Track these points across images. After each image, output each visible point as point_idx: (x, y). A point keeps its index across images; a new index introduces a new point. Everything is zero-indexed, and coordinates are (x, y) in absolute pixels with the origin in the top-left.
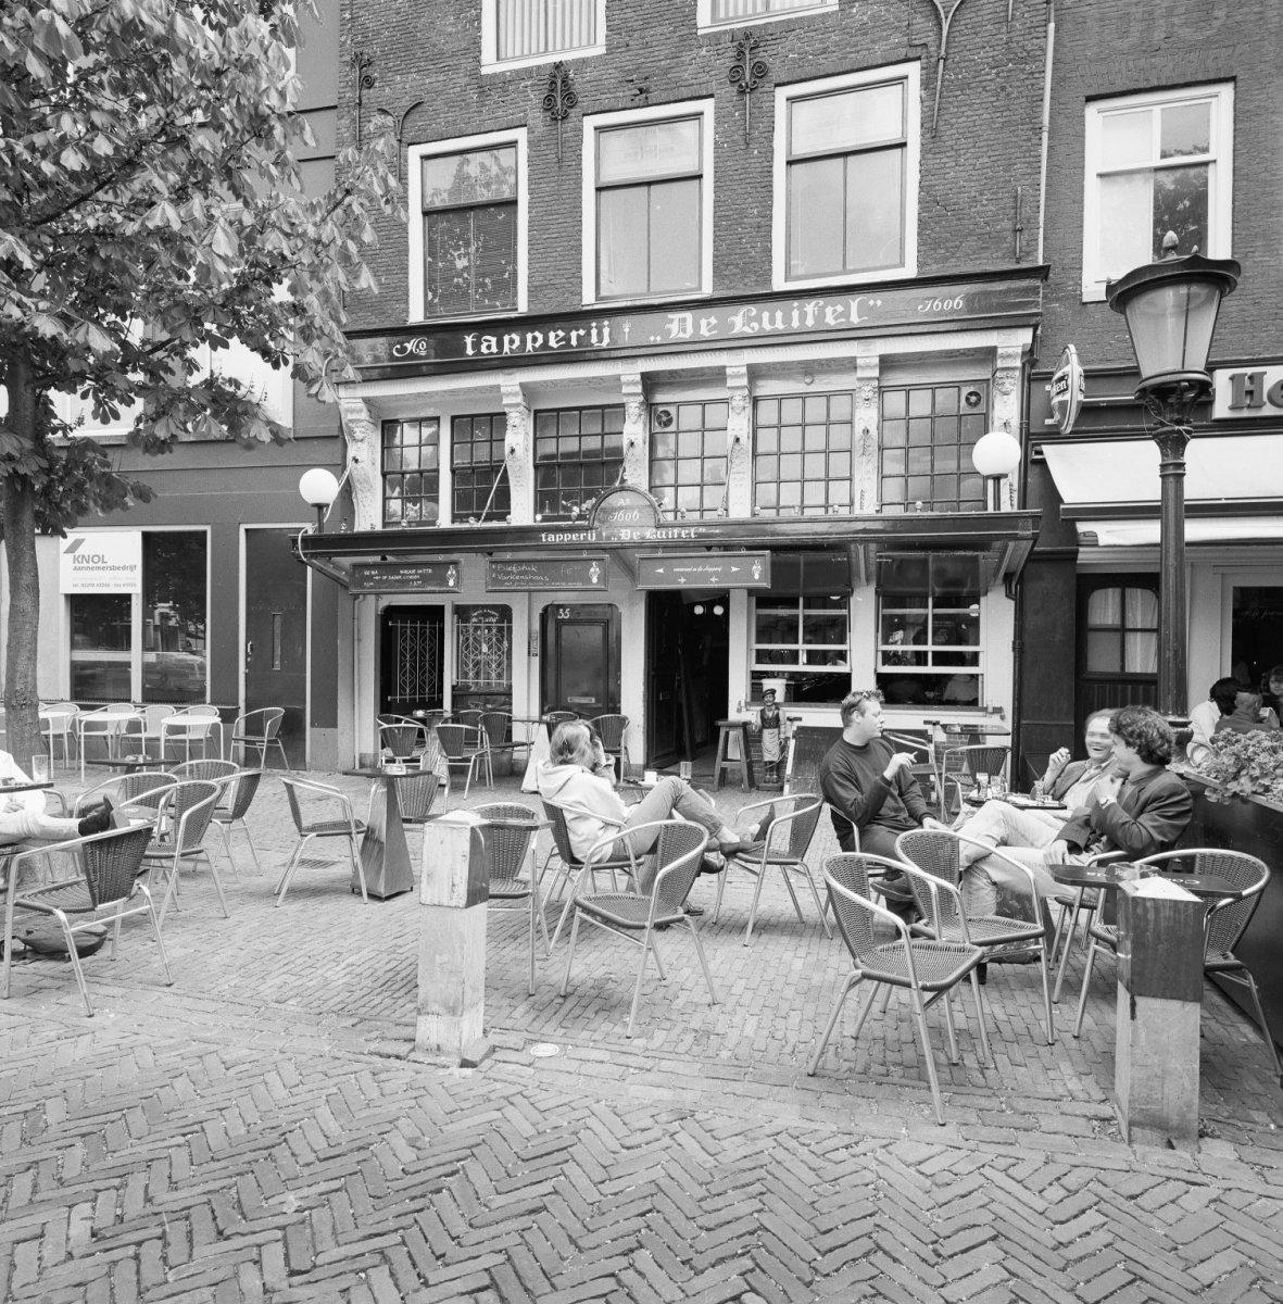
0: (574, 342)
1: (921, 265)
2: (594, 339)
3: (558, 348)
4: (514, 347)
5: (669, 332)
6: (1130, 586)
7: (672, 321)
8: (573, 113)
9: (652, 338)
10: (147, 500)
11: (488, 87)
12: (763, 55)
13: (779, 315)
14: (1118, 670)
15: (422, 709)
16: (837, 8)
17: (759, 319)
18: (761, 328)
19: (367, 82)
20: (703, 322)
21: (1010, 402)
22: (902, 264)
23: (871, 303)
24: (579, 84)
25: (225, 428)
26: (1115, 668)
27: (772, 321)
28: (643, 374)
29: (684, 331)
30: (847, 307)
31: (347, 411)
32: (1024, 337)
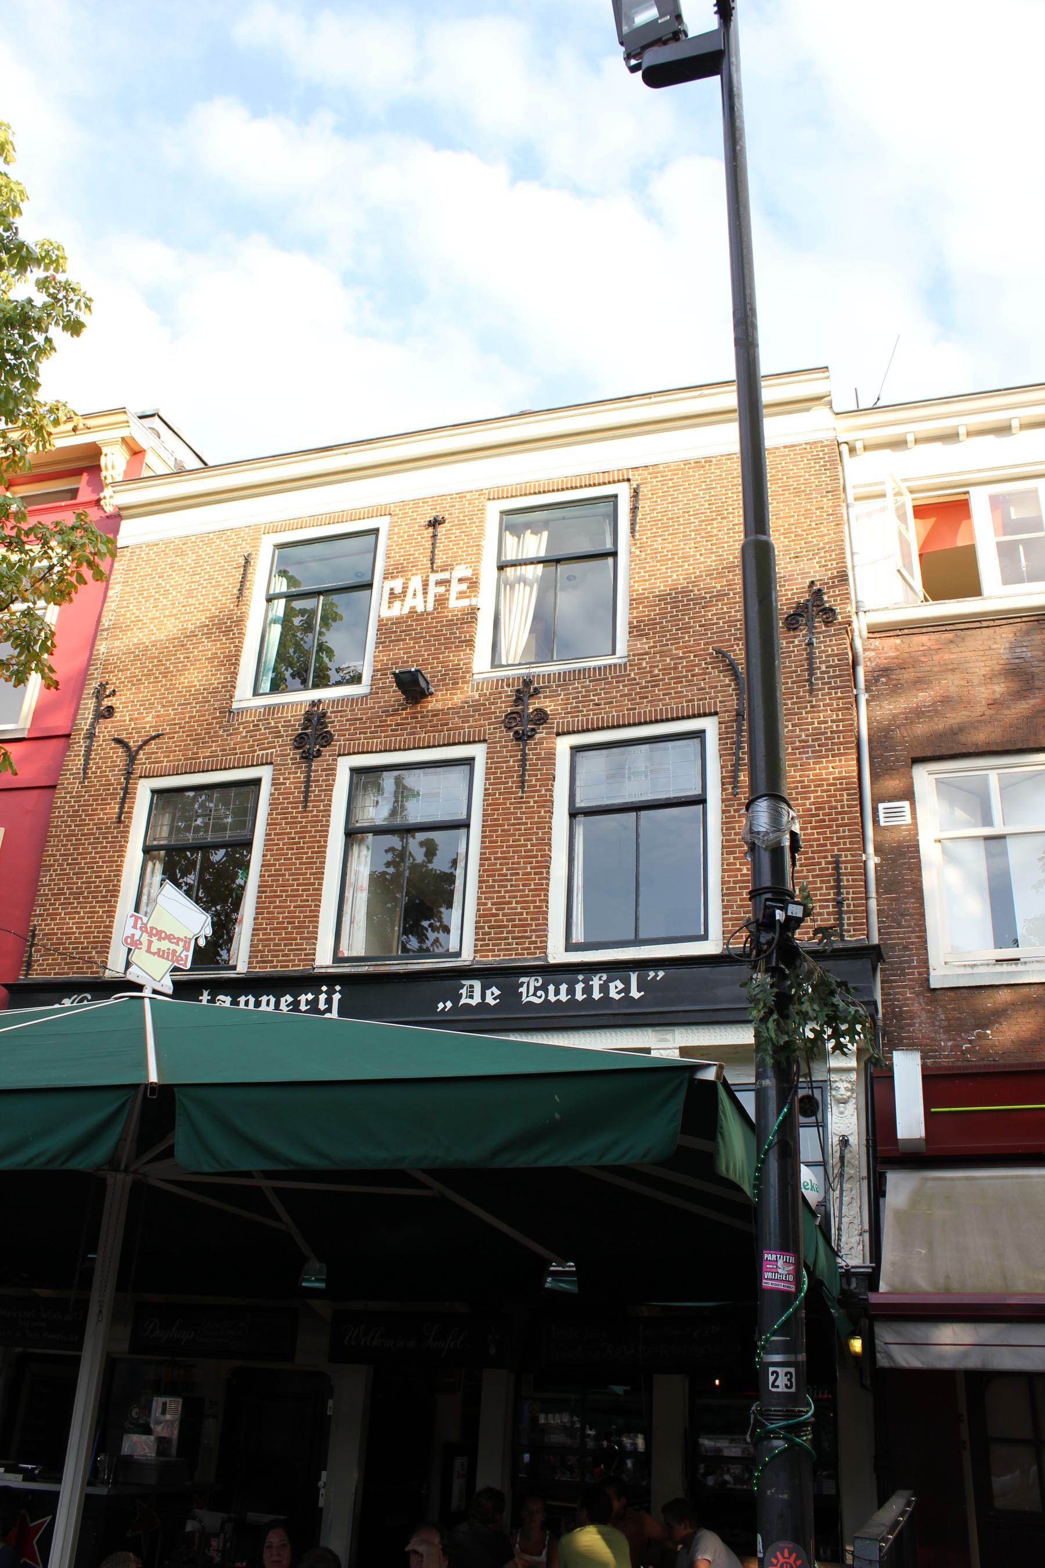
8: (326, 752)
9: (661, 974)
10: (442, 521)
18: (546, 1000)
21: (847, 1113)
24: (335, 725)
25: (542, 1421)
27: (557, 992)
28: (680, 1048)
29: (471, 997)
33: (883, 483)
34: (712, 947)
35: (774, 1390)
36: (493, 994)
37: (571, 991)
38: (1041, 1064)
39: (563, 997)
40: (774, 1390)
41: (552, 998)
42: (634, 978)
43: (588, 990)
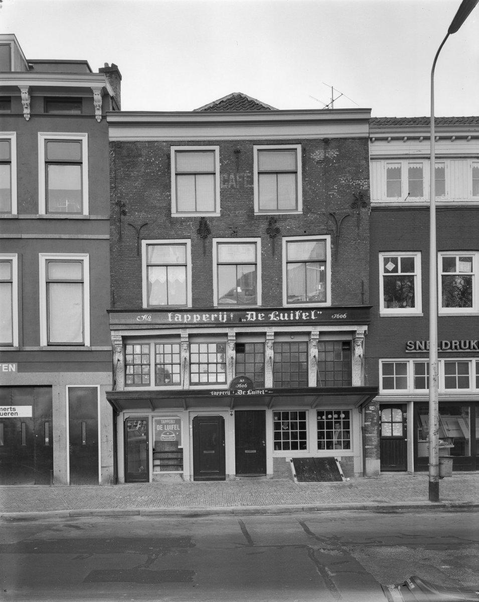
0: (213, 319)
1: (332, 302)
2: (220, 319)
3: (306, 320)
4: (189, 320)
5: (247, 318)
6: (395, 408)
7: (248, 314)
8: (209, 236)
11: (174, 222)
12: (278, 225)
13: (286, 315)
14: (391, 435)
15: (49, 440)
16: (302, 213)
17: (279, 315)
18: (280, 319)
19: (124, 213)
20: (259, 315)
22: (325, 301)
23: (318, 312)
26: (390, 435)
27: (284, 317)
28: (320, 332)
29: (253, 318)
30: (210, 316)
31: (115, 341)
32: (365, 328)
33: (428, 388)
34: (328, 304)
35: (456, 341)
36: (306, 315)
37: (289, 316)
38: (2, 484)
39: (286, 318)
40: (456, 341)
41: (282, 319)
42: (313, 313)
43: (295, 316)
